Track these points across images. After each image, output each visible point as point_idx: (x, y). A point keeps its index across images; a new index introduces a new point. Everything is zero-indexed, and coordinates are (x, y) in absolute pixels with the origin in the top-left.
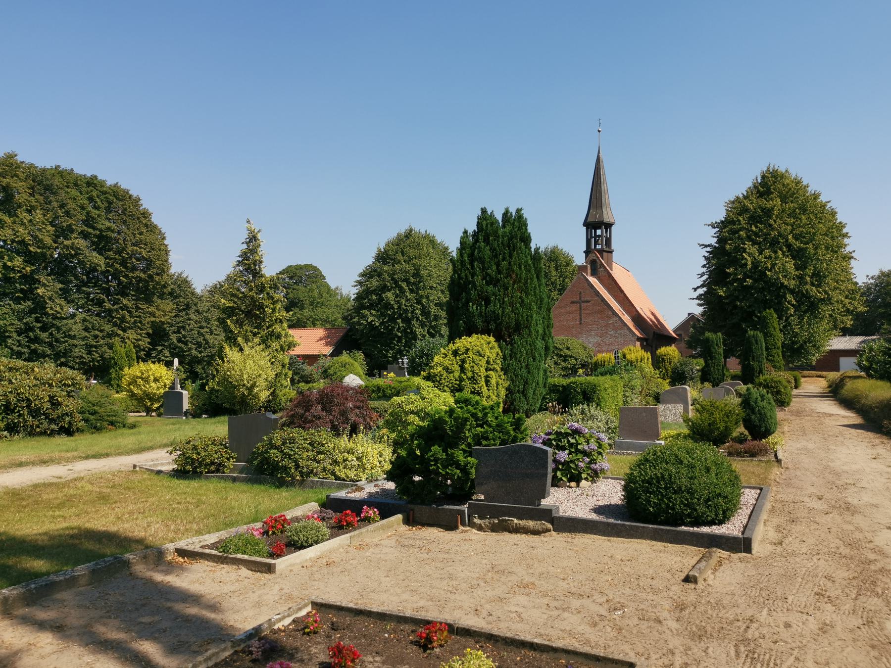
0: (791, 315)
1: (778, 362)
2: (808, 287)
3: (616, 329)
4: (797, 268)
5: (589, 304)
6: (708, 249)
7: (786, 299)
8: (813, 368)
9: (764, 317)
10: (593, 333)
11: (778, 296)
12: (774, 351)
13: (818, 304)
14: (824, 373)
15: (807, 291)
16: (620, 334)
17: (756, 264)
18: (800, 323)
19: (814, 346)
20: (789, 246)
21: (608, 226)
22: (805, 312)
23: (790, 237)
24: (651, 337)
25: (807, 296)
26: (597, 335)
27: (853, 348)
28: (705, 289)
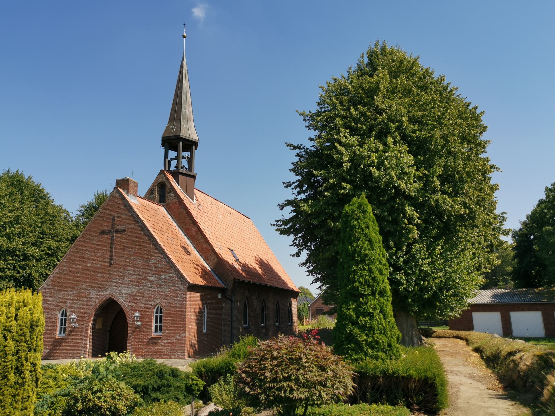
0: (415, 241)
1: (383, 332)
2: (438, 196)
3: (159, 272)
4: (418, 165)
5: (124, 235)
6: (298, 151)
10: (126, 279)
11: (392, 211)
12: (372, 302)
13: (455, 224)
14: (463, 333)
15: (437, 202)
16: (165, 280)
17: (356, 160)
19: (455, 295)
21: (190, 145)
22: (437, 238)
23: (405, 119)
24: (230, 286)
26: (131, 282)
28: (295, 214)
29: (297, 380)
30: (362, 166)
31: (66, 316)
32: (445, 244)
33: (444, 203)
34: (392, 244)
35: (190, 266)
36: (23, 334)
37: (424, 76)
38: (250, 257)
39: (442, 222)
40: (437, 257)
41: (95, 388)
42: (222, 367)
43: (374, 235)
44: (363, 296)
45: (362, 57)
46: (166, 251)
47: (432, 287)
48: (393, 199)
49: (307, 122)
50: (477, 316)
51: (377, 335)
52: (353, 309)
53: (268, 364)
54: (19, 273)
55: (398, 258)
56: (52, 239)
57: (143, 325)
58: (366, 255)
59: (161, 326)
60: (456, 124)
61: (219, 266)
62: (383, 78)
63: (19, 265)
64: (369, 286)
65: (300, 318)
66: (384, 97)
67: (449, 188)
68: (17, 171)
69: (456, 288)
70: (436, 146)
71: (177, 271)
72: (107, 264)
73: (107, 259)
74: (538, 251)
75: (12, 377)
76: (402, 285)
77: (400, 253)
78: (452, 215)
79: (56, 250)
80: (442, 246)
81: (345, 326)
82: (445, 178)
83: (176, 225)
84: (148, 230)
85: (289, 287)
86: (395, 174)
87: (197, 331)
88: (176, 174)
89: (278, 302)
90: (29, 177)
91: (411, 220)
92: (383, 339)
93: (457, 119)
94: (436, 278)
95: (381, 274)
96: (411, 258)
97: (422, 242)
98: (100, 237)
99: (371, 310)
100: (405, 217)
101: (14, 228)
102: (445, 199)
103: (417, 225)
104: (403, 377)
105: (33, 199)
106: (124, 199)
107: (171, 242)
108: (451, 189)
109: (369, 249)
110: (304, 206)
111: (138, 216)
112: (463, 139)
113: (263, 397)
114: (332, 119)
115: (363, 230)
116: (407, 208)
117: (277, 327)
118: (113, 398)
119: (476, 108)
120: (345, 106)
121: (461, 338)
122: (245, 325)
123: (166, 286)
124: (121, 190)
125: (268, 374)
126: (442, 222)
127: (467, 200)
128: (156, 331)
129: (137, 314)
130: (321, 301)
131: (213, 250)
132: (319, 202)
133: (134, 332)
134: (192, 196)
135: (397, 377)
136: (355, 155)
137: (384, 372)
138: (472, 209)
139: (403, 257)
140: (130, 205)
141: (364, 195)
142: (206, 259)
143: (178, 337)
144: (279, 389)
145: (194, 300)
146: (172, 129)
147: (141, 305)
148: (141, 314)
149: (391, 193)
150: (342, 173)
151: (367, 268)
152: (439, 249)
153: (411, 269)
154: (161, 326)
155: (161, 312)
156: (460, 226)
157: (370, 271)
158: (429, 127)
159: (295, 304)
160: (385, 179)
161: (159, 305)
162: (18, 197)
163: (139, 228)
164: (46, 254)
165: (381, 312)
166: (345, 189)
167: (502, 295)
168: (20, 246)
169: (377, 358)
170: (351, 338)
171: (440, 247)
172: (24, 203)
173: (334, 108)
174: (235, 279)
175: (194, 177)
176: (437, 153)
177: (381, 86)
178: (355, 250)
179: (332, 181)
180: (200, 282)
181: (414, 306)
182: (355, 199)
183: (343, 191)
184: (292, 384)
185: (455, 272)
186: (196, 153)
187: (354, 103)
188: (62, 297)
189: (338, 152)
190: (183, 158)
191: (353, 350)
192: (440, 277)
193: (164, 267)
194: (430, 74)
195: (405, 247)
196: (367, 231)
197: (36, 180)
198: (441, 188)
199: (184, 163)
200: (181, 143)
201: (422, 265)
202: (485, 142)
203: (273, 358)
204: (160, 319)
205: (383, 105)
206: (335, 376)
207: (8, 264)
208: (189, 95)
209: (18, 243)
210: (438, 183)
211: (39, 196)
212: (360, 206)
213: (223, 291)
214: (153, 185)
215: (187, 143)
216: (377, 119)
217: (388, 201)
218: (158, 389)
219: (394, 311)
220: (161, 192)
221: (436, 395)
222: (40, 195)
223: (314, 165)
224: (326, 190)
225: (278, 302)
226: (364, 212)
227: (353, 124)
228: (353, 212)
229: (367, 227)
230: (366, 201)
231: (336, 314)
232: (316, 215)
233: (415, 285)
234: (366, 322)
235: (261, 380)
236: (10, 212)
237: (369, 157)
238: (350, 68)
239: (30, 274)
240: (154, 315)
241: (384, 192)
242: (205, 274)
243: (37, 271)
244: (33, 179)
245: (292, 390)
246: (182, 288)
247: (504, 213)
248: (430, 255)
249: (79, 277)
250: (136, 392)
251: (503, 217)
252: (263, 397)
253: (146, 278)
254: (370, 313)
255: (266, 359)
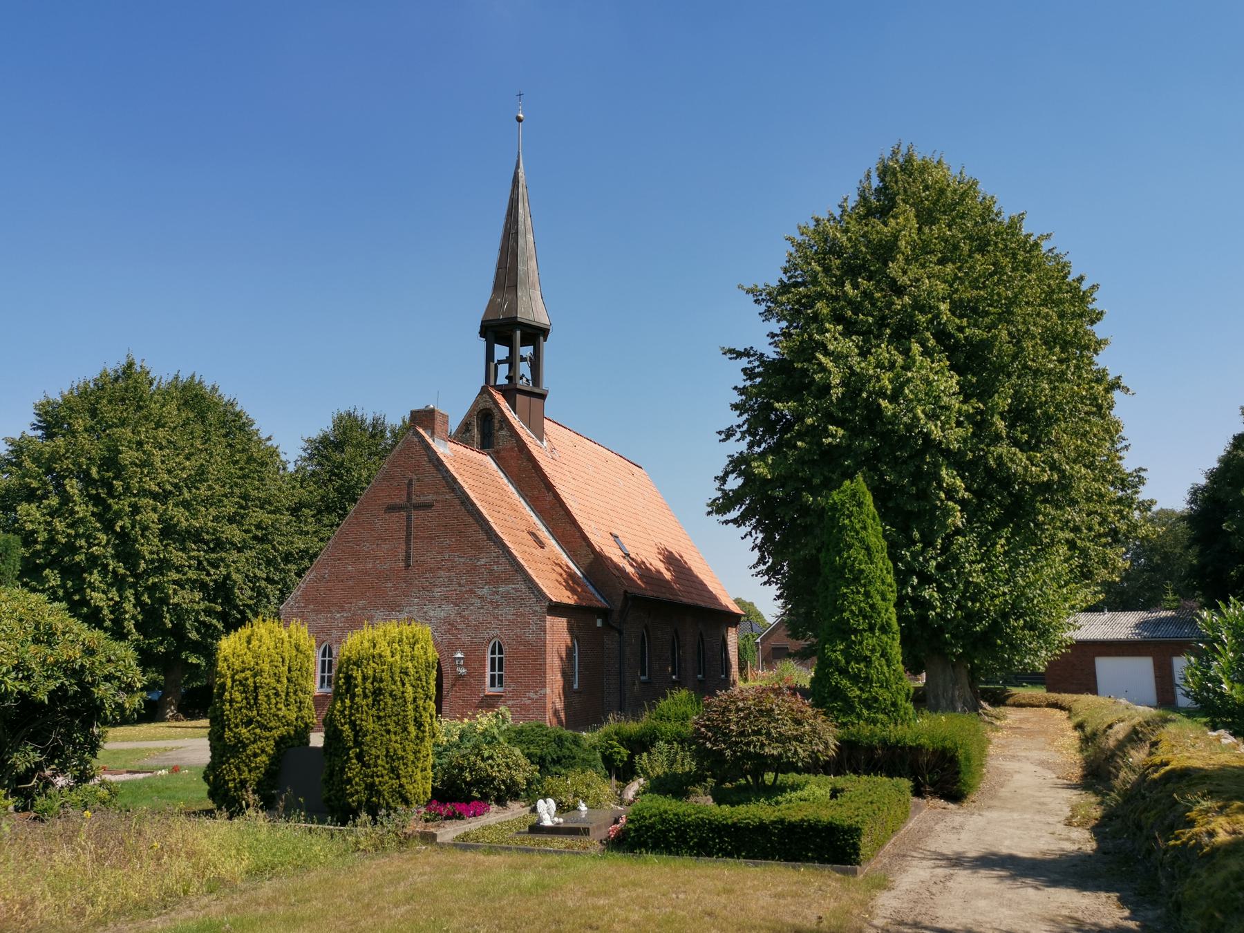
0: (958, 532)
1: (885, 685)
2: (1003, 449)
3: (494, 580)
4: (966, 393)
5: (431, 513)
6: (744, 362)
7: (940, 481)
8: (1034, 679)
9: (834, 508)
10: (437, 593)
11: (917, 476)
12: (870, 641)
14: (1066, 698)
16: (506, 596)
17: (854, 383)
18: (985, 557)
19: (1031, 627)
20: (942, 335)
21: (535, 334)
22: (997, 525)
23: (943, 307)
24: (618, 604)
25: (1000, 478)
26: (446, 598)
27: (1122, 636)
29: (768, 734)
30: (864, 395)
31: (330, 655)
32: (1013, 535)
33: (1012, 460)
34: (916, 535)
35: (547, 565)
36: (419, 679)
37: (983, 218)
38: (650, 549)
39: (1010, 494)
40: (997, 557)
41: (486, 754)
42: (644, 735)
43: (874, 539)
44: (855, 632)
45: (868, 177)
46: (509, 544)
47: (988, 611)
48: (921, 454)
49: (764, 304)
50: (1105, 667)
51: (876, 689)
52: (841, 651)
53: (733, 716)
54: (208, 574)
55: (927, 561)
56: (262, 508)
57: (469, 674)
58: (862, 571)
59: (501, 676)
60: (1038, 314)
61: (596, 569)
62: (905, 223)
63: (207, 560)
64: (865, 617)
65: (742, 668)
66: (907, 260)
67: (1023, 433)
68: (193, 376)
69: (1033, 614)
70: (999, 356)
71: (528, 580)
72: (402, 564)
73: (402, 555)
74: (1232, 533)
75: (412, 728)
76: (934, 608)
77: (931, 552)
78: (1028, 483)
79: (271, 530)
80: (1007, 539)
81: (828, 677)
82: (1017, 415)
83: (513, 490)
84: (473, 505)
85: (714, 598)
86: (924, 412)
87: (564, 689)
88: (510, 392)
89: (701, 634)
90: (213, 388)
91: (951, 493)
92: (884, 695)
93: (1040, 305)
94: (996, 596)
95: (884, 599)
96: (950, 560)
97: (972, 531)
98: (387, 516)
99: (868, 653)
100: (940, 487)
101: (198, 489)
102: (1015, 454)
103: (963, 503)
104: (911, 747)
105: (223, 431)
106: (428, 447)
107: (512, 525)
108: (1026, 437)
109: (866, 563)
110: (758, 467)
111: (454, 479)
112: (1051, 339)
113: (728, 753)
114: (811, 300)
115: (857, 533)
116: (944, 472)
117: (700, 681)
118: (508, 766)
119: (1080, 279)
120: (835, 276)
121: (1062, 708)
122: (643, 678)
123: (509, 604)
124: (421, 431)
125: (734, 727)
126: (1010, 494)
127: (1056, 456)
128: (493, 685)
129: (459, 655)
130: (783, 632)
131: (585, 538)
132: (786, 458)
133: (453, 685)
134: (540, 434)
135: (903, 748)
136: (853, 373)
137: (884, 741)
138: (1064, 471)
139: (935, 559)
140: (438, 459)
141: (859, 477)
142: (572, 554)
143: (532, 695)
144: (748, 744)
145: (558, 631)
146: (501, 305)
147: (465, 638)
148: (466, 654)
149: (916, 443)
150: (827, 408)
151: (862, 590)
152: (1002, 546)
153: (951, 580)
154: (501, 676)
155: (501, 652)
156: (1042, 502)
157: (867, 595)
158: (987, 320)
159: (733, 638)
160: (905, 419)
161: (497, 640)
162: (198, 428)
163: (457, 502)
164: (255, 538)
165: (882, 656)
166: (834, 436)
167: (1159, 622)
168: (210, 524)
169: (875, 722)
170: (838, 693)
171: (1003, 541)
172: (209, 439)
173: (815, 282)
174: (626, 592)
175: (542, 397)
176: (1001, 369)
177: (902, 244)
178: (845, 563)
179: (809, 421)
180: (566, 598)
181: (956, 646)
182: (847, 483)
183: (830, 440)
184: (762, 738)
185: (1029, 585)
186: (547, 347)
187: (852, 271)
188: (322, 622)
189: (823, 369)
190: (523, 359)
191: (839, 711)
192: (1004, 594)
193: (505, 571)
194: (993, 216)
195: (940, 541)
196: (863, 534)
197: (227, 393)
198: (1008, 433)
199: (524, 369)
200: (518, 333)
201: (970, 573)
202: (1099, 343)
203: (738, 710)
204: (497, 664)
205: (905, 278)
206: (814, 731)
207: (190, 558)
208: (530, 237)
209: (204, 519)
210: (1001, 425)
211: (234, 426)
212: (854, 495)
213: (604, 613)
214: (469, 415)
215: (529, 331)
216: (894, 303)
217: (910, 457)
218: (557, 761)
219: (903, 654)
220: (484, 428)
221: (958, 773)
222: (238, 424)
223: (776, 390)
224: (800, 436)
225: (701, 634)
226: (860, 504)
227: (850, 313)
228: (843, 505)
229: (864, 528)
230: (864, 487)
231: (815, 660)
232: (780, 481)
233: (957, 609)
234: (859, 670)
235: (724, 734)
236: (188, 459)
237: (878, 379)
238: (846, 200)
239: (228, 577)
240: (489, 656)
241: (904, 441)
242: (570, 581)
243: (238, 571)
244: (220, 392)
245: (763, 745)
246: (538, 609)
247: (1141, 469)
248: (985, 557)
249: (352, 588)
250: (532, 763)
251: (1139, 477)
252: (728, 753)
253: (471, 591)
254: (866, 657)
255: (730, 711)
